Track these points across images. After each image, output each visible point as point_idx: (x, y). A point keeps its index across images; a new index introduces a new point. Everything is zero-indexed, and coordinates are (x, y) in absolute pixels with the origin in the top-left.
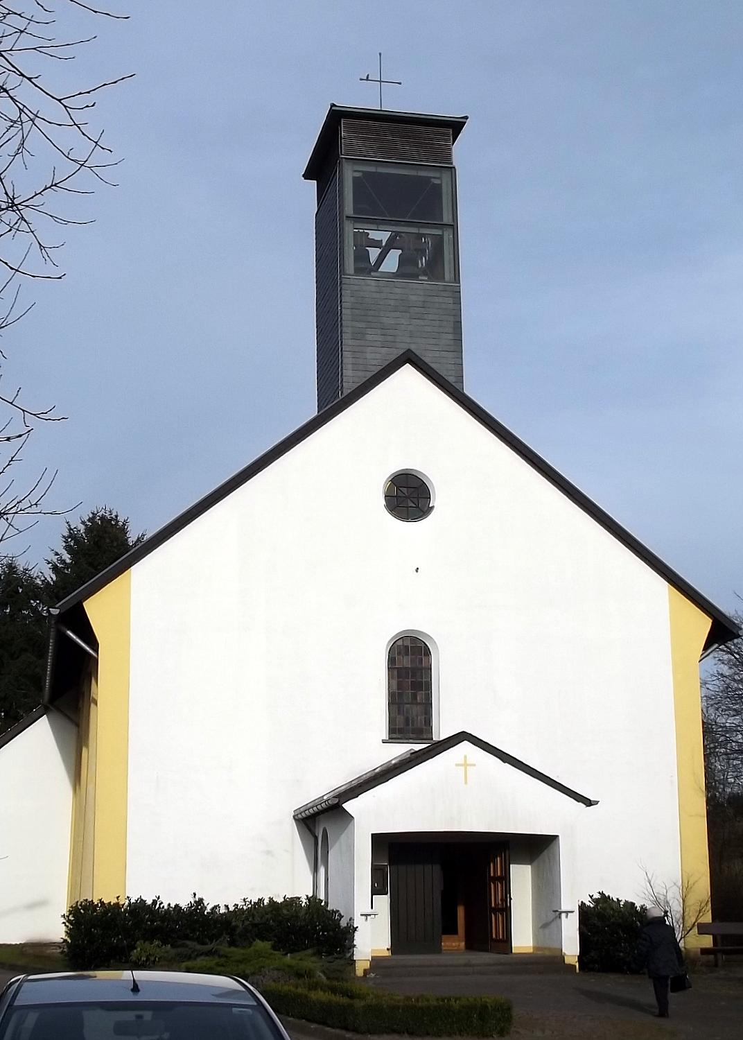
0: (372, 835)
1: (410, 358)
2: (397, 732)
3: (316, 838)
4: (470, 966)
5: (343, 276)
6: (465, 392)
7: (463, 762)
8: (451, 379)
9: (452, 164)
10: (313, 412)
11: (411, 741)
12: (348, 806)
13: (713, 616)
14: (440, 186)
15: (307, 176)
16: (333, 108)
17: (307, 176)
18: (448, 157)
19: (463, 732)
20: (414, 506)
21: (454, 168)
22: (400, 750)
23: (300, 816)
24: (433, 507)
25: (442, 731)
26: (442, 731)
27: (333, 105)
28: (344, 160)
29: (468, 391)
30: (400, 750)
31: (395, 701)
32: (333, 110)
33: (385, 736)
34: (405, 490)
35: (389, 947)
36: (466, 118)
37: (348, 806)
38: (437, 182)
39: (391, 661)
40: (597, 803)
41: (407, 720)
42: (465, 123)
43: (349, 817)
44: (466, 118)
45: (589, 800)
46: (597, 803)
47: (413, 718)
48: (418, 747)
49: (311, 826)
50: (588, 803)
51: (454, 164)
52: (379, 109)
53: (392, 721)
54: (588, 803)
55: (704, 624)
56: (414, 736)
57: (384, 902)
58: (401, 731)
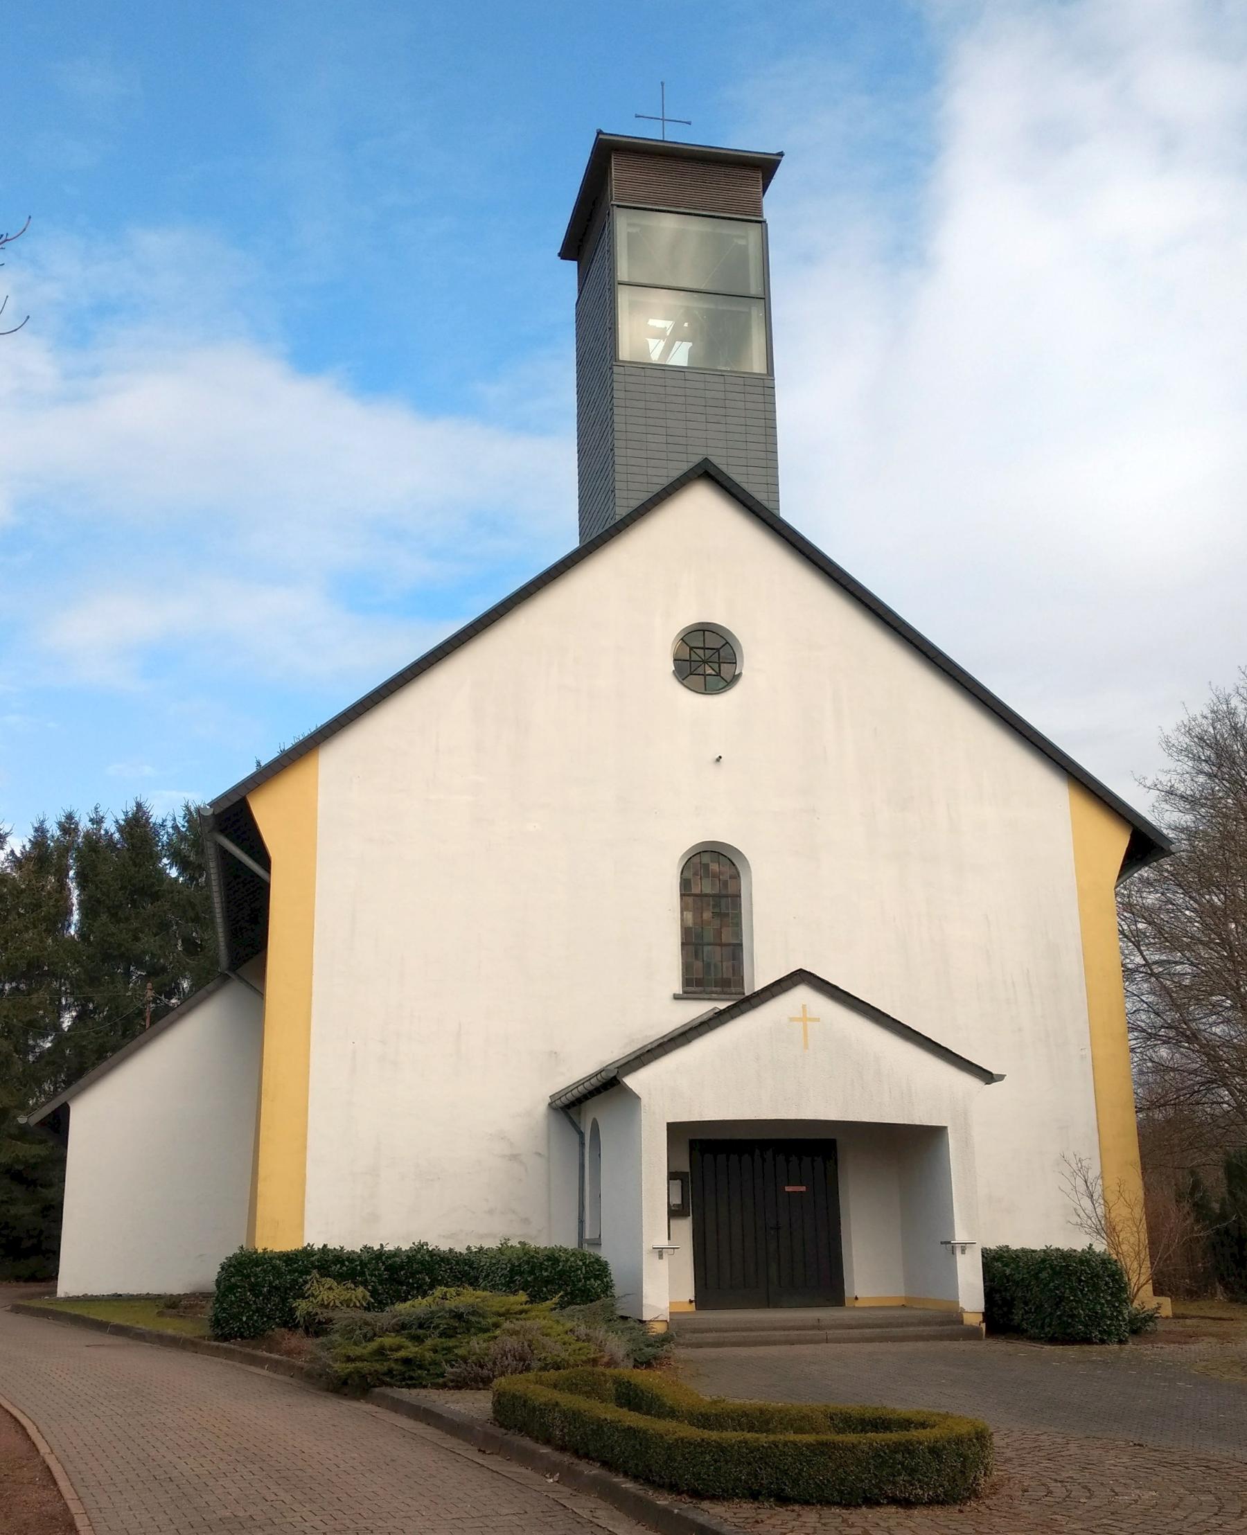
0: (668, 1124)
1: (708, 474)
2: (694, 985)
3: (581, 1135)
4: (819, 1328)
5: (614, 363)
6: (781, 515)
7: (799, 1015)
8: (760, 496)
9: (762, 216)
10: (574, 543)
11: (714, 996)
12: (631, 1081)
13: (1133, 825)
14: (746, 247)
15: (565, 254)
16: (601, 136)
17: (565, 254)
18: (758, 210)
19: (801, 970)
20: (714, 673)
21: (765, 222)
22: (698, 1009)
23: (558, 1102)
24: (740, 674)
25: (761, 975)
26: (761, 975)
27: (600, 132)
28: (615, 207)
29: (788, 513)
30: (698, 1009)
31: (692, 942)
32: (601, 139)
33: (678, 988)
34: (700, 652)
35: (693, 1299)
36: (781, 154)
37: (631, 1081)
38: (742, 242)
39: (685, 885)
40: (1001, 1077)
41: (707, 966)
42: (779, 161)
43: (633, 1098)
44: (781, 154)
45: (991, 1073)
46: (1001, 1077)
47: (715, 966)
48: (722, 1006)
49: (575, 1118)
50: (988, 1077)
51: (764, 218)
52: (662, 139)
53: (687, 968)
54: (988, 1077)
55: (1117, 842)
56: (718, 989)
57: (685, 1227)
58: (699, 983)
